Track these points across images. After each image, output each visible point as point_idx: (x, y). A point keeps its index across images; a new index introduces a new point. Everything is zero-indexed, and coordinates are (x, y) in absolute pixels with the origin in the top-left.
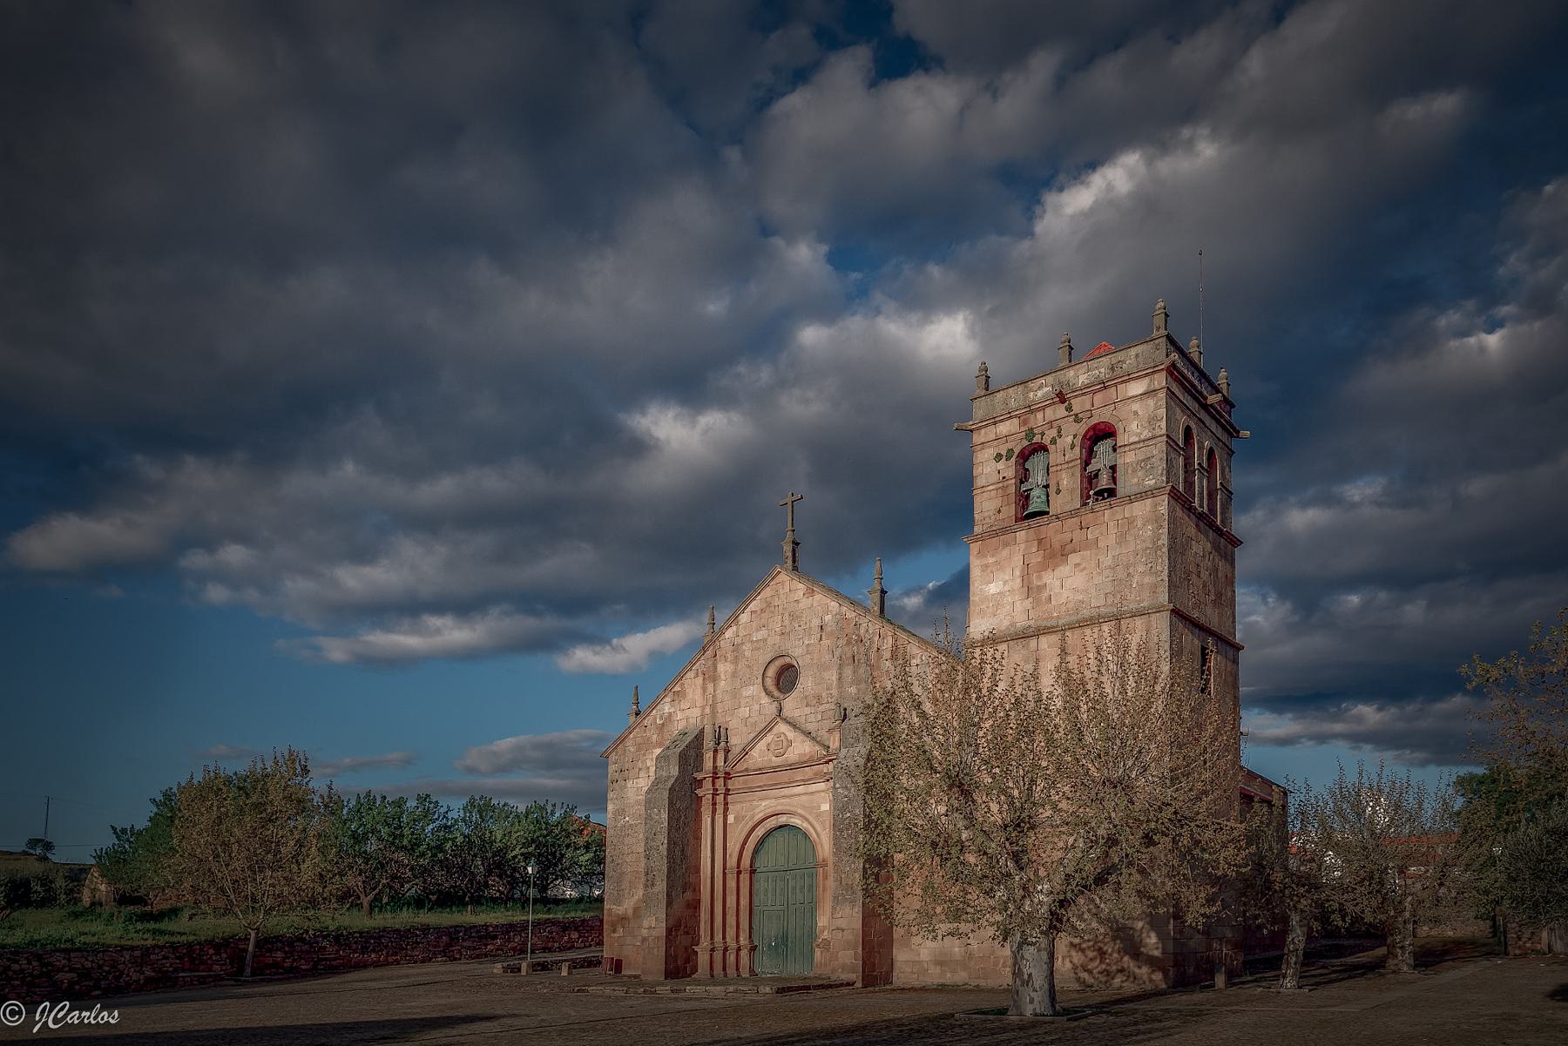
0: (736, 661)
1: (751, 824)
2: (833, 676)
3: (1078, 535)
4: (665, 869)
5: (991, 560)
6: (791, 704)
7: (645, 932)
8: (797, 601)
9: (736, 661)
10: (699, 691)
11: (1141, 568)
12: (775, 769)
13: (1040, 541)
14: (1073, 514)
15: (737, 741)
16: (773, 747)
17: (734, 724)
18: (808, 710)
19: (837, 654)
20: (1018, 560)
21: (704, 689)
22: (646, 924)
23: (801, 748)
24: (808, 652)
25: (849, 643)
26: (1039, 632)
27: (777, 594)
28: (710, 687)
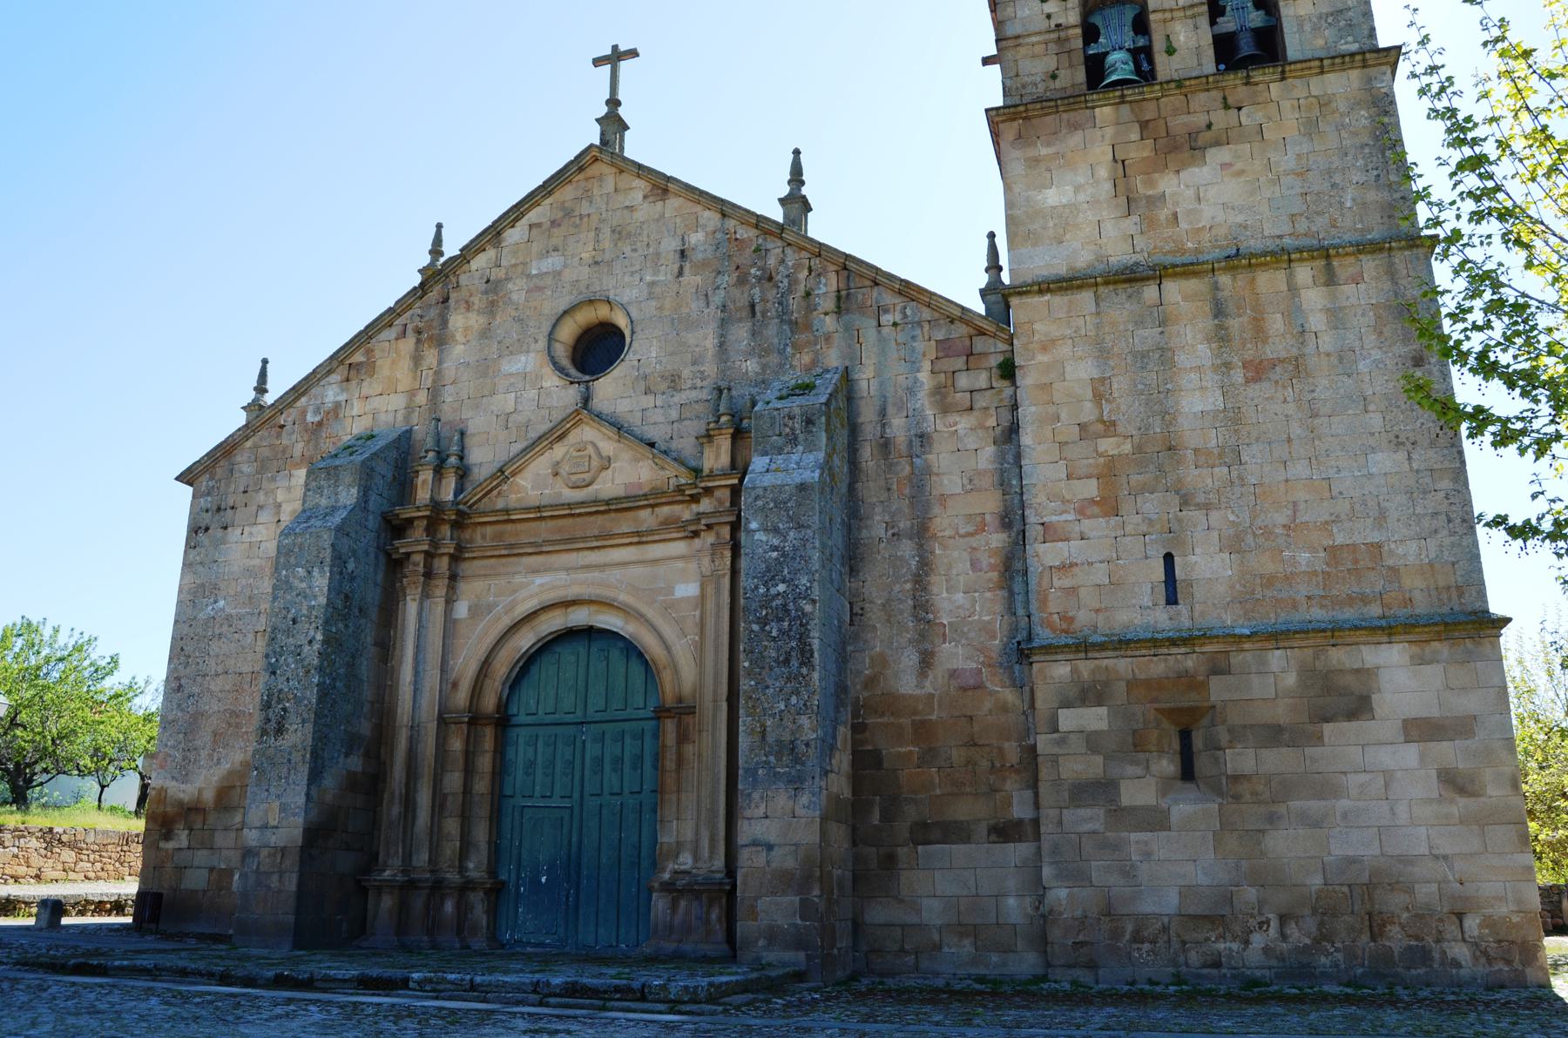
0: (491, 309)
1: (506, 622)
2: (707, 340)
3: (1220, 119)
4: (312, 696)
5: (1044, 151)
6: (610, 389)
7: (251, 837)
8: (630, 208)
9: (491, 309)
10: (406, 363)
11: (1357, 177)
12: (571, 511)
13: (1144, 125)
14: (1204, 83)
15: (483, 458)
16: (565, 469)
17: (478, 423)
18: (648, 401)
19: (717, 299)
20: (1101, 153)
21: (417, 360)
22: (255, 815)
23: (630, 472)
24: (651, 296)
25: (742, 281)
26: (1159, 273)
27: (587, 195)
28: (430, 357)
